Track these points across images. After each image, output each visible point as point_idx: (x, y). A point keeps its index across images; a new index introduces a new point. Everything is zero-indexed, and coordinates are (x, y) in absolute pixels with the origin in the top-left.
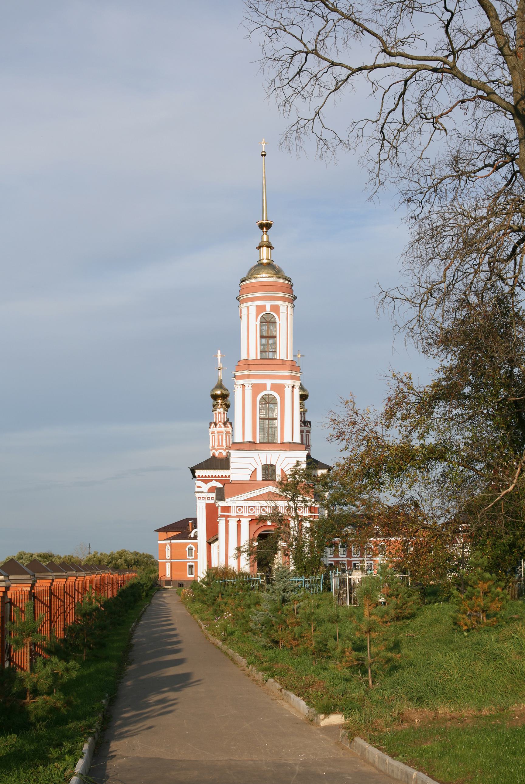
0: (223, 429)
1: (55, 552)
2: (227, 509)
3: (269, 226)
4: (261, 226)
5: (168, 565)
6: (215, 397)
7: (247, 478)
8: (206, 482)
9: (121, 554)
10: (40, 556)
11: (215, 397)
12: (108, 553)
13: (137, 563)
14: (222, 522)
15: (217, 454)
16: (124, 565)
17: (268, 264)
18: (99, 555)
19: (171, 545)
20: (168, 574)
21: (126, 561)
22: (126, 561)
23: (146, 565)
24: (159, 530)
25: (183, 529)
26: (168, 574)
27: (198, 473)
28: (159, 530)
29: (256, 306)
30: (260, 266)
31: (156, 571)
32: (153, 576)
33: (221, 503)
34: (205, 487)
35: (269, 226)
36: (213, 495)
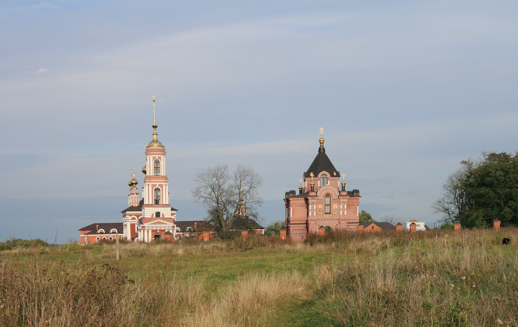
3: (156, 127)
4: (154, 127)
8: (130, 216)
19: (88, 237)
27: (127, 212)
35: (156, 127)
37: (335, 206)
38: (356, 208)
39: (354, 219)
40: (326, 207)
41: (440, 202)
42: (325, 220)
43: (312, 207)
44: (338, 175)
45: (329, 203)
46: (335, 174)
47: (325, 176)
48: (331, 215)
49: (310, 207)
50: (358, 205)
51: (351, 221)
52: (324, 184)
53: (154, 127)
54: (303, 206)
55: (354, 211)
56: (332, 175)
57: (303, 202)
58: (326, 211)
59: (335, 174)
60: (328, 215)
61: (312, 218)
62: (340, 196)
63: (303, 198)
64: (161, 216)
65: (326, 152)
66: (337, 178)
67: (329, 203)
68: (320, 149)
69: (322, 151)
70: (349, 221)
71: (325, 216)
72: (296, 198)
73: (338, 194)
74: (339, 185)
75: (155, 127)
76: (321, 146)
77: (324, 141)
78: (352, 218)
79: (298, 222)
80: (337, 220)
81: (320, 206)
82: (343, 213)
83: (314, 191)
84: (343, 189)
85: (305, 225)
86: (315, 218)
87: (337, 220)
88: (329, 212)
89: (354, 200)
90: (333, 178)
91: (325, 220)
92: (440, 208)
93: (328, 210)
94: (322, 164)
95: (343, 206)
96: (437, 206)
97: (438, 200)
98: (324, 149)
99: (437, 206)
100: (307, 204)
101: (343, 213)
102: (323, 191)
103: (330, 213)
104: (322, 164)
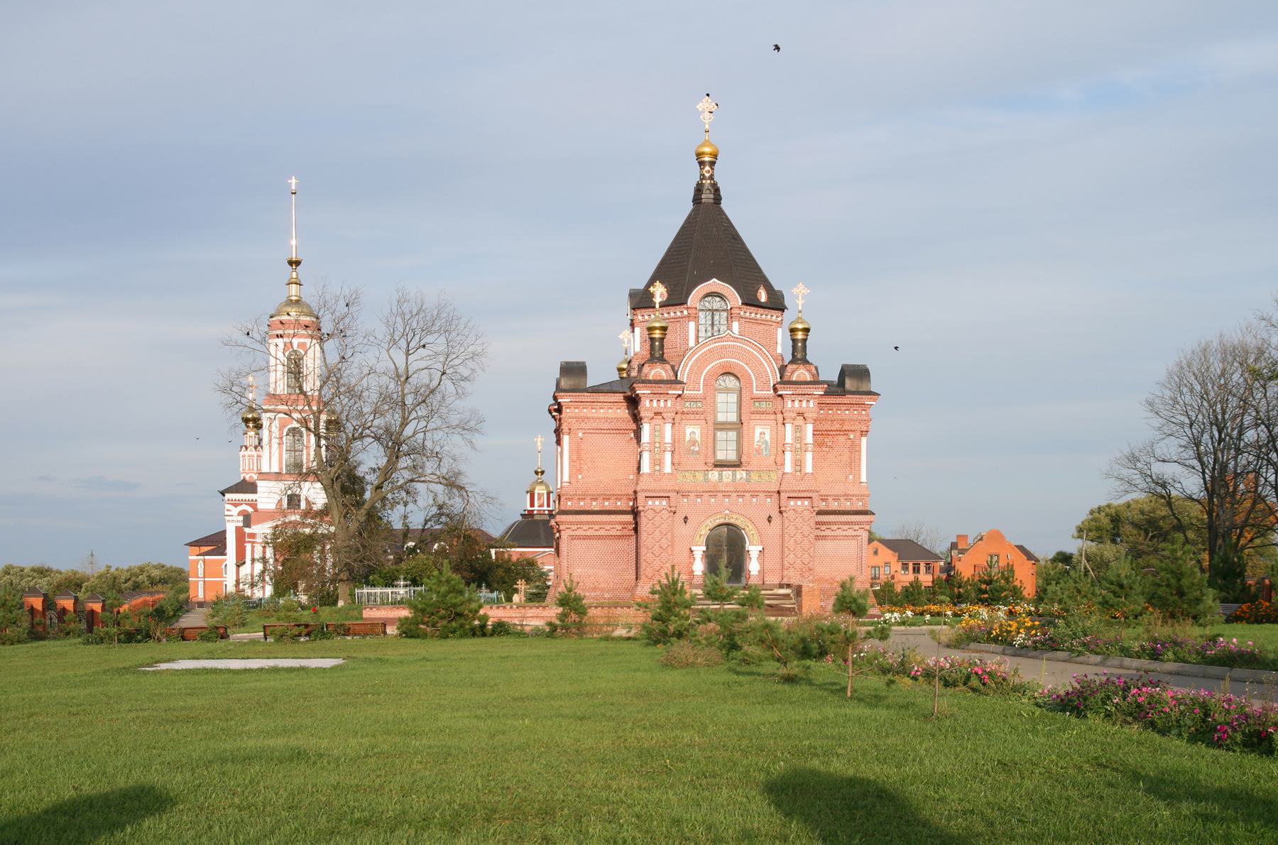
0: (254, 453)
1: (55, 567)
2: (253, 535)
3: (298, 263)
4: (291, 263)
5: (201, 584)
6: (246, 421)
7: (273, 507)
8: (236, 505)
9: (142, 570)
10: (33, 570)
11: (246, 421)
12: (126, 568)
13: (163, 581)
14: (248, 547)
15: (247, 478)
16: (147, 583)
17: (297, 301)
18: (112, 570)
19: (204, 561)
20: (201, 595)
21: (149, 577)
22: (149, 577)
23: (175, 581)
24: (191, 544)
25: (215, 543)
26: (201, 595)
27: (228, 496)
28: (191, 544)
29: (224, 532)
30: (290, 303)
31: (186, 590)
32: (182, 597)
33: (247, 530)
34: (235, 511)
35: (298, 263)
36: (241, 518)
37: (761, 433)
38: (854, 448)
39: (847, 497)
40: (720, 435)
41: (1133, 459)
42: (713, 493)
43: (652, 435)
44: (777, 303)
45: (733, 417)
46: (763, 296)
47: (716, 303)
48: (741, 474)
49: (646, 429)
50: (864, 433)
51: (834, 506)
52: (710, 327)
53: (291, 263)
54: (618, 431)
55: (846, 457)
56: (750, 301)
57: (623, 412)
58: (721, 456)
59: (763, 296)
60: (727, 474)
61: (653, 485)
62: (784, 382)
63: (620, 397)
64: (303, 505)
65: (723, 205)
66: (773, 316)
67: (733, 417)
68: (699, 190)
69: (707, 197)
70: (823, 506)
71: (714, 475)
72: (586, 397)
73: (774, 377)
74: (783, 345)
75: (295, 263)
76: (703, 177)
77: (715, 156)
78: (838, 490)
79: (595, 506)
80: (768, 494)
81: (693, 431)
82: (799, 464)
83: (662, 360)
84: (799, 355)
85: (629, 518)
86: (667, 484)
87: (768, 494)
88: (732, 456)
89: (844, 412)
90: (751, 313)
91: (713, 493)
92: (1138, 479)
93: (726, 452)
94: (707, 251)
95: (798, 429)
96: (1125, 472)
97: (1127, 451)
98: (716, 190)
99: (1125, 472)
100: (637, 419)
101: (799, 464)
102: (704, 360)
103: (737, 465)
104: (707, 251)
